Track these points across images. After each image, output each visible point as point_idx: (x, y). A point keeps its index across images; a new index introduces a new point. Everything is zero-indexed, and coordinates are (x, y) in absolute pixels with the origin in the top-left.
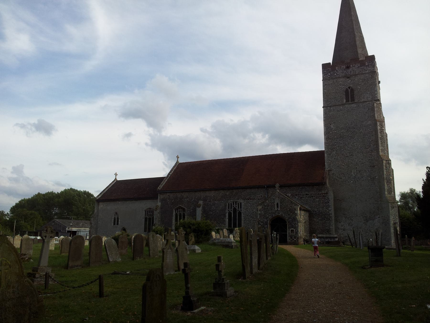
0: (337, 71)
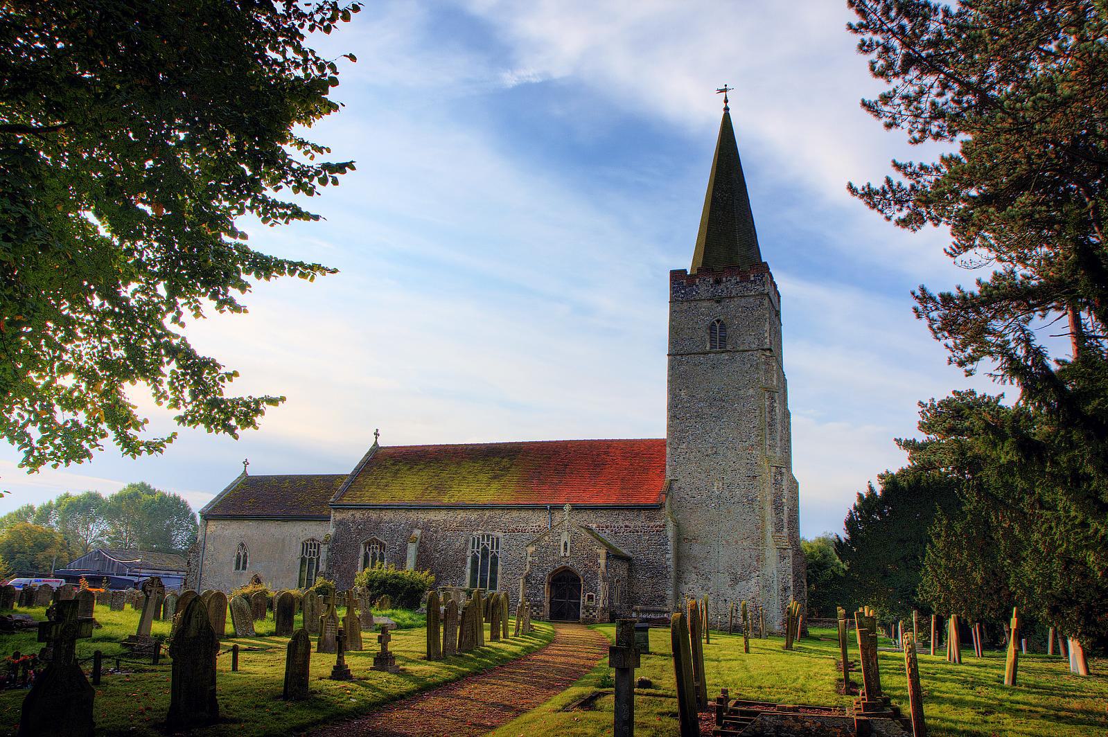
0: (697, 286)
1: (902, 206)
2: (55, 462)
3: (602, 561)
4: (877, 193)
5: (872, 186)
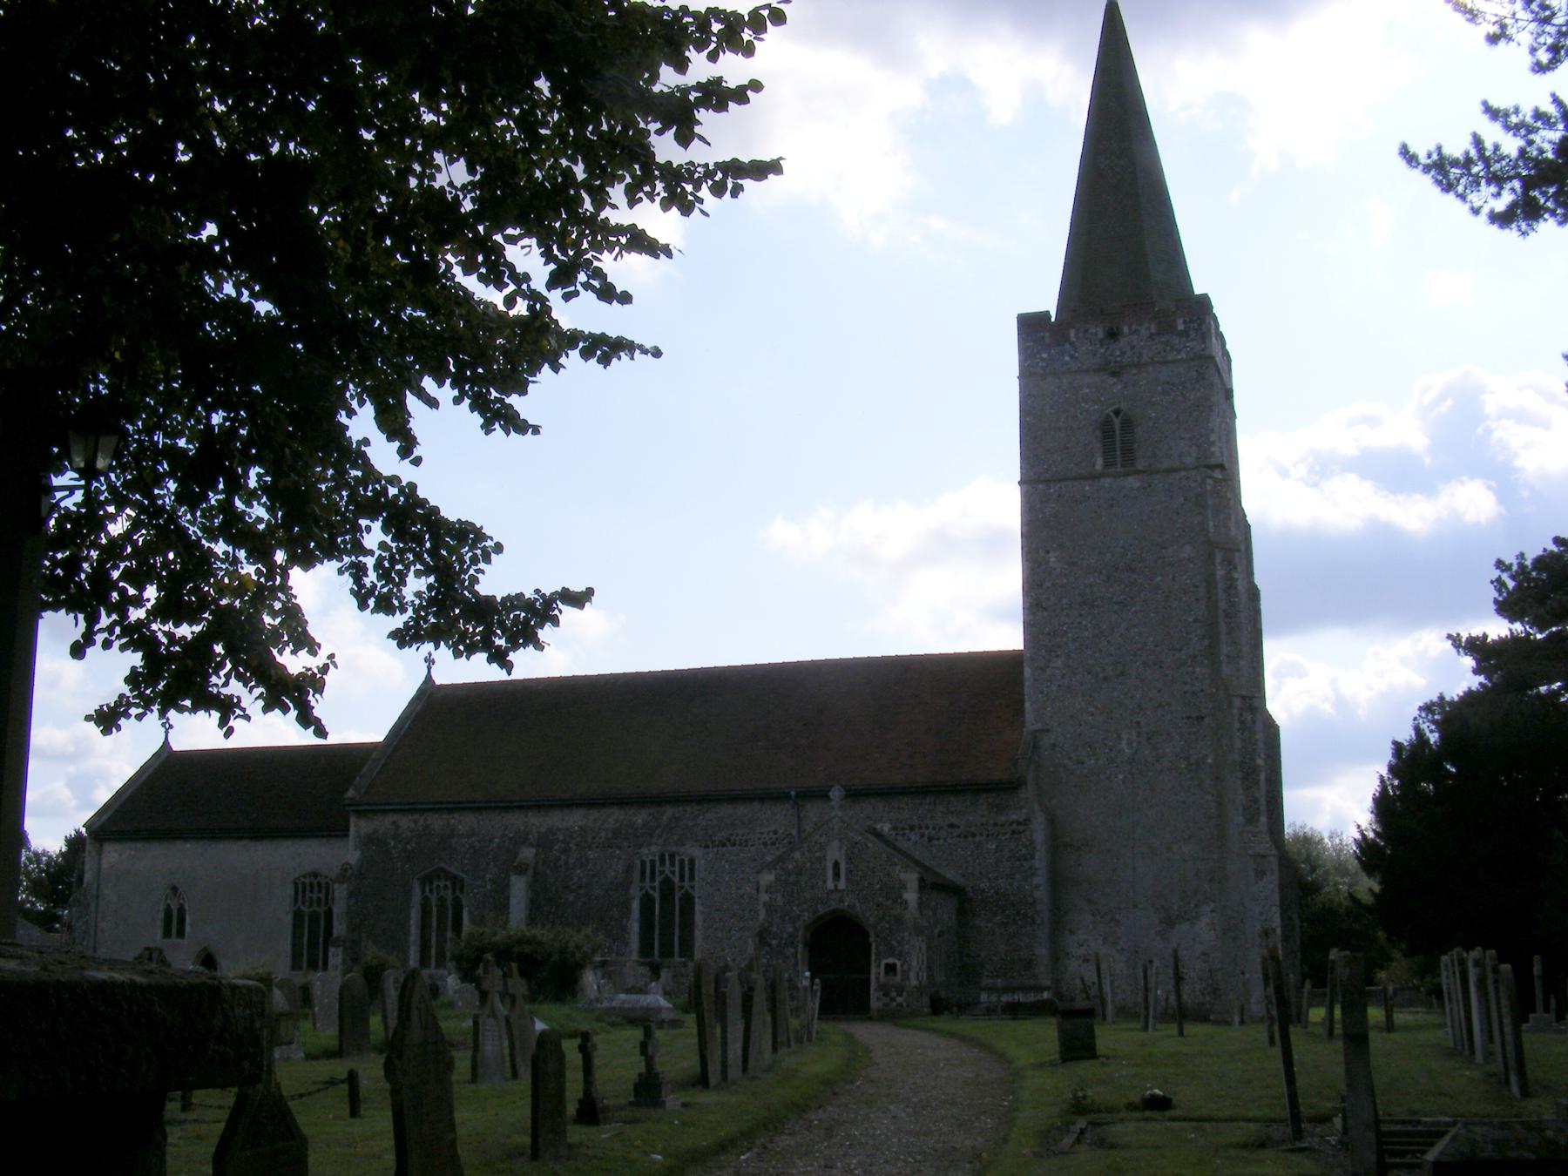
1: (1501, 188)
2: (140, 710)
3: (911, 896)
4: (1455, 163)
5: (1447, 151)
